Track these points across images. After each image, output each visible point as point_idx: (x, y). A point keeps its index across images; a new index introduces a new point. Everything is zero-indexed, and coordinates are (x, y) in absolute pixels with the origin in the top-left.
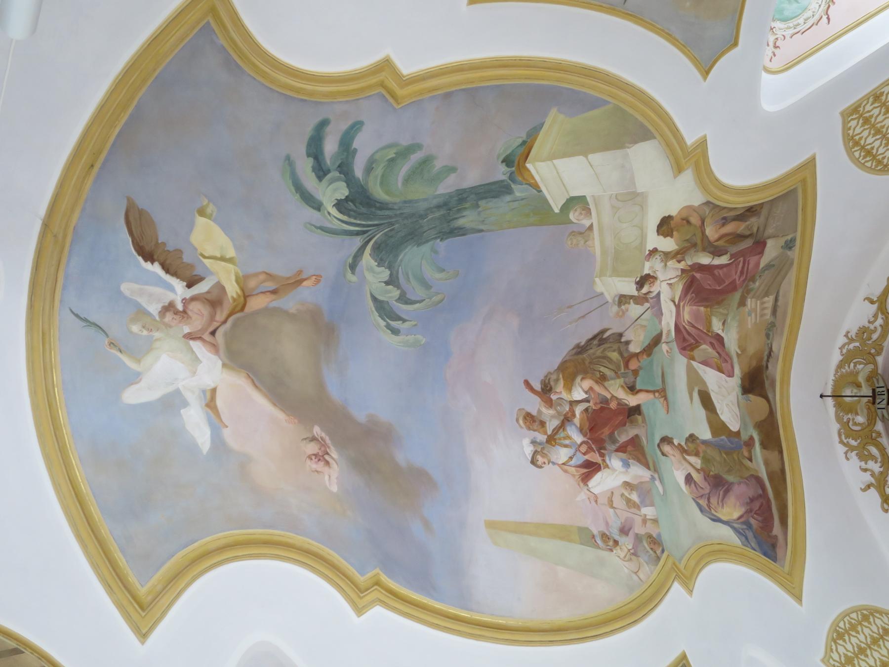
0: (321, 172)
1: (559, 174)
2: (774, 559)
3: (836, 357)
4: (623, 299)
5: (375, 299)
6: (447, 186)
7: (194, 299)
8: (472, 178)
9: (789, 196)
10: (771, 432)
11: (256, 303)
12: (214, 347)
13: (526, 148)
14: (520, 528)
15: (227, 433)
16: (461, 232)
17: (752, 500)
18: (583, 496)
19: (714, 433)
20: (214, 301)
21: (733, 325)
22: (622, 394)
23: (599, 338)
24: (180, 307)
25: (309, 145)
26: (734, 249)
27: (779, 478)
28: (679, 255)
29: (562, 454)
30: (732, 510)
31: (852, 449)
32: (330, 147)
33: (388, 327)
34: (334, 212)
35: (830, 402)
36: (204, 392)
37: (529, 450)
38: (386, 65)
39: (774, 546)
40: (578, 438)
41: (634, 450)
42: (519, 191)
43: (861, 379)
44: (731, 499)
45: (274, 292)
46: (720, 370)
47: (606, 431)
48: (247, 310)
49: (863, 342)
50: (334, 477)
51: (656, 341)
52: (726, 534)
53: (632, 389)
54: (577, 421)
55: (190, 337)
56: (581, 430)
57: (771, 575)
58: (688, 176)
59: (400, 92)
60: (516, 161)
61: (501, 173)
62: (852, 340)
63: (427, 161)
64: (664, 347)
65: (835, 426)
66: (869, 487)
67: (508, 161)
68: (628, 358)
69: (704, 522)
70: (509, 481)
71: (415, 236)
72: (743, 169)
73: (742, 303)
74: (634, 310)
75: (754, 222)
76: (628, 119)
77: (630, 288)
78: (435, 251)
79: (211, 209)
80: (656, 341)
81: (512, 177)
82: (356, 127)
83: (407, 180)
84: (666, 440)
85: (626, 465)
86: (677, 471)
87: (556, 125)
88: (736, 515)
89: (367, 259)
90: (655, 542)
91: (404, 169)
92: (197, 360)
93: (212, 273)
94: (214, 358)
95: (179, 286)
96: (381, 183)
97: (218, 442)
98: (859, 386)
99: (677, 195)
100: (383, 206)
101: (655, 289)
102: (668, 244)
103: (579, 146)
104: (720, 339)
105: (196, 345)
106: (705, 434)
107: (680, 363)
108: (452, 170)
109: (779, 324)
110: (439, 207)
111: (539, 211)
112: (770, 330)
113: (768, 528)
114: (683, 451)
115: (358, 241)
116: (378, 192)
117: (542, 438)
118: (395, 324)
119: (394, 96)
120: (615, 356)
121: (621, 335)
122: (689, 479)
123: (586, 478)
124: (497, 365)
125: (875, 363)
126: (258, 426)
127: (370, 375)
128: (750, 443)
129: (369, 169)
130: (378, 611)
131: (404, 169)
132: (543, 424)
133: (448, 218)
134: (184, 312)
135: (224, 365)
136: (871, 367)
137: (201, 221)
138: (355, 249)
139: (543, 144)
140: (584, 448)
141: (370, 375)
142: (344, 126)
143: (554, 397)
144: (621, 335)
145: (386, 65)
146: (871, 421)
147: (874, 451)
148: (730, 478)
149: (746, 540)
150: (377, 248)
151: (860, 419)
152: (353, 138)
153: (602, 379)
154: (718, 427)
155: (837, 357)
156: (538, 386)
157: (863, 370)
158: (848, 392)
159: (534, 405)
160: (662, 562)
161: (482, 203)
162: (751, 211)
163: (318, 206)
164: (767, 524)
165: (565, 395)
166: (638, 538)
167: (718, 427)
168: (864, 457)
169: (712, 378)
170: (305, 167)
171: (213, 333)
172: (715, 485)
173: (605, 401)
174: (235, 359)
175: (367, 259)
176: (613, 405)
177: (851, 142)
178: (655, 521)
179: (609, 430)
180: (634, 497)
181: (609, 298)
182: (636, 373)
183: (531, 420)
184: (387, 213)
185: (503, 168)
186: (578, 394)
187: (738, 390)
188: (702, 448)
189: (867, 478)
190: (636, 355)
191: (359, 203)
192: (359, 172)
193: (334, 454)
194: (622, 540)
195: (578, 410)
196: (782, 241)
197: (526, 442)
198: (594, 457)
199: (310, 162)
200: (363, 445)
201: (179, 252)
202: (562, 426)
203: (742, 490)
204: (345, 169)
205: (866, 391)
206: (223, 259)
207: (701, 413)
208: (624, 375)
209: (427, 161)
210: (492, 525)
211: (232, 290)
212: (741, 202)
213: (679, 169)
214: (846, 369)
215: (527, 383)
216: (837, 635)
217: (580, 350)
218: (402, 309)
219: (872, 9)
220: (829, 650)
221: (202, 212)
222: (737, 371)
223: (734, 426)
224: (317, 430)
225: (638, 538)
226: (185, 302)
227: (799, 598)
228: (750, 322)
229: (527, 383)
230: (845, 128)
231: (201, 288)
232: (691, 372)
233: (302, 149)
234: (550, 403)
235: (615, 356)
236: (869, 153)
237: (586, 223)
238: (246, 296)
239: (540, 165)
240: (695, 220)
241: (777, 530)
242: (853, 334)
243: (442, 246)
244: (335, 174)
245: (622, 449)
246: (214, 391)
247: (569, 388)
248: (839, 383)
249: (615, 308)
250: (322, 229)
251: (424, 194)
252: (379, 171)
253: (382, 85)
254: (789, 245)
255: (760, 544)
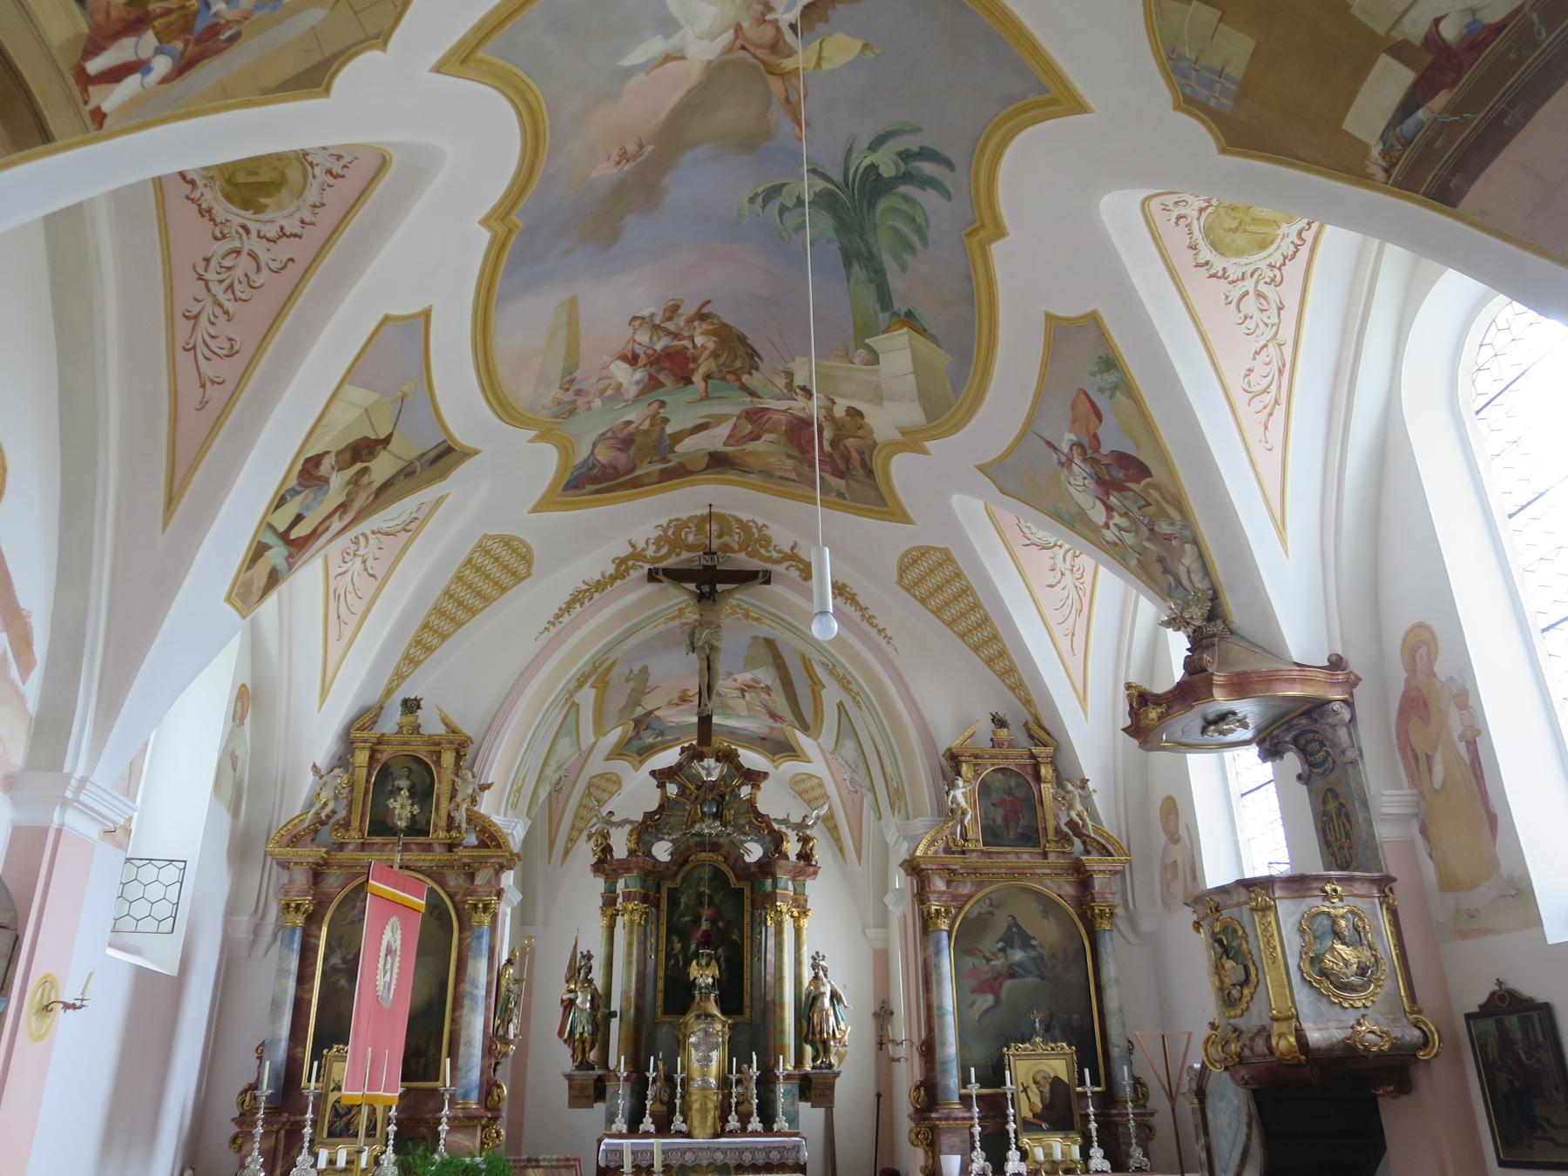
0: (906, 156)
1: (898, 353)
2: (566, 488)
3: (745, 517)
4: (790, 375)
5: (783, 185)
6: (887, 259)
7: (778, 29)
8: (896, 283)
9: (881, 500)
10: (677, 473)
11: (776, 85)
12: (729, 50)
13: (922, 331)
14: (572, 323)
15: (641, 76)
16: (848, 264)
17: (614, 468)
18: (606, 358)
19: (671, 436)
20: (777, 47)
21: (771, 448)
22: (702, 370)
23: (753, 354)
24: (769, 17)
25: (932, 150)
26: (836, 456)
27: (636, 484)
28: (830, 417)
29: (643, 337)
30: (603, 455)
31: (665, 531)
32: (928, 168)
33: (757, 194)
34: (867, 162)
35: (707, 511)
36: (682, 50)
37: (645, 313)
38: (1001, 233)
39: (575, 487)
40: (659, 346)
41: (652, 384)
42: (884, 317)
43: (726, 538)
44: (613, 454)
45: (787, 100)
46: (730, 437)
47: (667, 364)
48: (768, 76)
49: (758, 540)
50: (605, 171)
51: (753, 394)
52: (584, 452)
53: (707, 377)
54: (676, 343)
55: (738, 29)
56: (667, 347)
57: (551, 490)
58: (898, 436)
59: (975, 240)
60: (908, 319)
61: (900, 306)
62: (760, 530)
63: (911, 249)
64: (748, 399)
65: (684, 516)
66: (633, 546)
67: (909, 314)
68: (737, 375)
69: (593, 437)
70: (617, 303)
71: (843, 227)
72: (904, 473)
73: (789, 456)
74: (781, 382)
75: (861, 473)
76: (945, 406)
77: (799, 380)
78: (829, 241)
79: (870, 55)
80: (753, 394)
81: (895, 314)
82: (947, 194)
83: (895, 230)
84: (663, 404)
85: (637, 383)
86: (637, 415)
87: (942, 359)
88: (600, 458)
89: (821, 185)
90: (571, 412)
91: (905, 229)
92: (713, 38)
93: (804, 46)
94: (718, 51)
95: (794, 16)
96: (892, 208)
97: (630, 72)
98: (720, 536)
99: (883, 422)
100: (872, 206)
101: (799, 398)
102: (839, 411)
103: (921, 368)
104: (757, 438)
105: (730, 34)
106: (669, 429)
107: (737, 410)
108: (903, 268)
109: (770, 479)
110: (870, 251)
111: (864, 330)
112: (767, 474)
113: (589, 481)
114: (653, 417)
115: (839, 178)
116: (884, 203)
117: (657, 321)
118: (759, 200)
119: (971, 234)
120: (738, 364)
121: (757, 369)
122: (629, 423)
123: (623, 358)
124: (727, 282)
125: (739, 551)
126: (648, 102)
127: (709, 183)
128: (664, 460)
129: (906, 198)
130: (486, 236)
131: (905, 229)
132: (670, 319)
133: (857, 257)
134: (764, 21)
135: (710, 62)
136: (736, 547)
137: (859, 45)
138: (830, 175)
139: (923, 344)
140: (650, 352)
141: (709, 183)
142: (947, 183)
143: (696, 323)
144: (757, 369)
145: (1001, 233)
146: (690, 548)
147: (664, 550)
148: (633, 451)
149: (577, 468)
150: (831, 194)
151: (691, 538)
152: (935, 189)
153: (715, 355)
154: (678, 437)
155: (745, 517)
156: (705, 310)
157: (733, 540)
158: (714, 527)
159: (688, 310)
160: (551, 424)
161: (873, 286)
162: (870, 472)
163: (874, 147)
164: (595, 480)
165: (698, 331)
166: (574, 402)
167: (678, 437)
168: (659, 542)
169: (723, 431)
170: (912, 143)
171: (743, 48)
172: (626, 441)
173: (695, 359)
174: (716, 72)
175: (821, 185)
176: (691, 366)
177: (924, 551)
178: (589, 409)
179: (670, 367)
180: (609, 392)
181: (790, 365)
182: (724, 379)
183: (673, 311)
184: (865, 207)
185: (904, 309)
186: (699, 341)
187: (712, 449)
188: (658, 428)
189: (641, 545)
190: (739, 379)
191: (874, 185)
192: (904, 189)
193: (627, 167)
194: (571, 393)
195: (686, 343)
196: (843, 490)
197: (653, 310)
198: (643, 360)
199: (915, 148)
200: (644, 178)
201: (827, 20)
202: (668, 333)
203: (622, 459)
204: (908, 177)
205: (715, 544)
206: (820, 58)
207: (690, 425)
208: (720, 371)
209: (911, 249)
210: (573, 302)
211: (788, 64)
212: (877, 466)
213: (904, 432)
214: (734, 525)
215: (708, 302)
216: (507, 541)
217: (742, 339)
218: (774, 207)
219: (1206, 328)
220: (494, 537)
221: (866, 46)
222: (729, 449)
223: (678, 448)
224: (650, 148)
225: (574, 402)
226: (775, 23)
227: (534, 510)
228: (772, 460)
229: (708, 302)
230: (936, 549)
231: (788, 36)
232: (727, 417)
233: (928, 143)
234: (690, 321)
235: (738, 364)
236: (915, 562)
237: (856, 360)
238: (783, 75)
239: (906, 338)
240: (860, 433)
241: (589, 488)
242: (765, 531)
243: (835, 246)
244: (903, 168)
245: (651, 377)
246: (683, 58)
247: (706, 333)
248: (721, 518)
249: (781, 368)
250: (850, 150)
251: (883, 245)
252: (904, 207)
253: (982, 226)
254: (840, 495)
255: (577, 477)
